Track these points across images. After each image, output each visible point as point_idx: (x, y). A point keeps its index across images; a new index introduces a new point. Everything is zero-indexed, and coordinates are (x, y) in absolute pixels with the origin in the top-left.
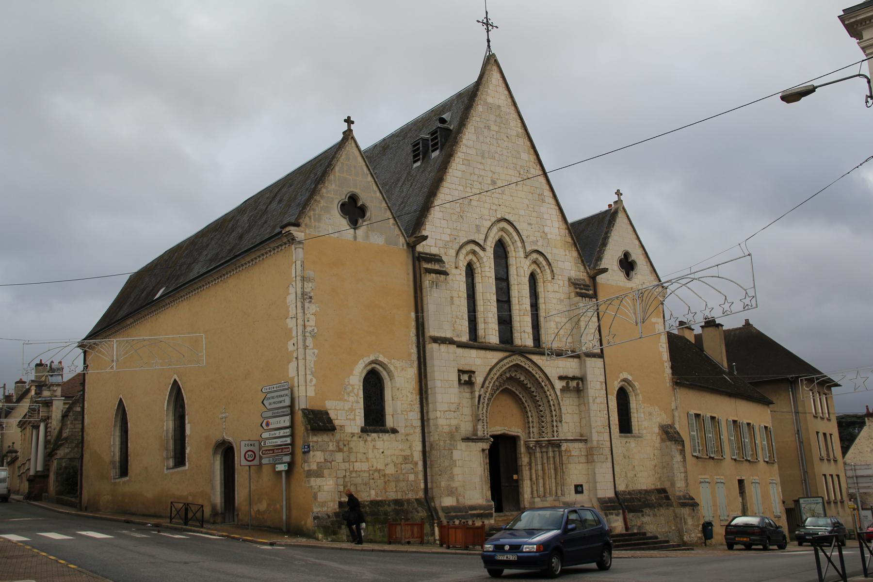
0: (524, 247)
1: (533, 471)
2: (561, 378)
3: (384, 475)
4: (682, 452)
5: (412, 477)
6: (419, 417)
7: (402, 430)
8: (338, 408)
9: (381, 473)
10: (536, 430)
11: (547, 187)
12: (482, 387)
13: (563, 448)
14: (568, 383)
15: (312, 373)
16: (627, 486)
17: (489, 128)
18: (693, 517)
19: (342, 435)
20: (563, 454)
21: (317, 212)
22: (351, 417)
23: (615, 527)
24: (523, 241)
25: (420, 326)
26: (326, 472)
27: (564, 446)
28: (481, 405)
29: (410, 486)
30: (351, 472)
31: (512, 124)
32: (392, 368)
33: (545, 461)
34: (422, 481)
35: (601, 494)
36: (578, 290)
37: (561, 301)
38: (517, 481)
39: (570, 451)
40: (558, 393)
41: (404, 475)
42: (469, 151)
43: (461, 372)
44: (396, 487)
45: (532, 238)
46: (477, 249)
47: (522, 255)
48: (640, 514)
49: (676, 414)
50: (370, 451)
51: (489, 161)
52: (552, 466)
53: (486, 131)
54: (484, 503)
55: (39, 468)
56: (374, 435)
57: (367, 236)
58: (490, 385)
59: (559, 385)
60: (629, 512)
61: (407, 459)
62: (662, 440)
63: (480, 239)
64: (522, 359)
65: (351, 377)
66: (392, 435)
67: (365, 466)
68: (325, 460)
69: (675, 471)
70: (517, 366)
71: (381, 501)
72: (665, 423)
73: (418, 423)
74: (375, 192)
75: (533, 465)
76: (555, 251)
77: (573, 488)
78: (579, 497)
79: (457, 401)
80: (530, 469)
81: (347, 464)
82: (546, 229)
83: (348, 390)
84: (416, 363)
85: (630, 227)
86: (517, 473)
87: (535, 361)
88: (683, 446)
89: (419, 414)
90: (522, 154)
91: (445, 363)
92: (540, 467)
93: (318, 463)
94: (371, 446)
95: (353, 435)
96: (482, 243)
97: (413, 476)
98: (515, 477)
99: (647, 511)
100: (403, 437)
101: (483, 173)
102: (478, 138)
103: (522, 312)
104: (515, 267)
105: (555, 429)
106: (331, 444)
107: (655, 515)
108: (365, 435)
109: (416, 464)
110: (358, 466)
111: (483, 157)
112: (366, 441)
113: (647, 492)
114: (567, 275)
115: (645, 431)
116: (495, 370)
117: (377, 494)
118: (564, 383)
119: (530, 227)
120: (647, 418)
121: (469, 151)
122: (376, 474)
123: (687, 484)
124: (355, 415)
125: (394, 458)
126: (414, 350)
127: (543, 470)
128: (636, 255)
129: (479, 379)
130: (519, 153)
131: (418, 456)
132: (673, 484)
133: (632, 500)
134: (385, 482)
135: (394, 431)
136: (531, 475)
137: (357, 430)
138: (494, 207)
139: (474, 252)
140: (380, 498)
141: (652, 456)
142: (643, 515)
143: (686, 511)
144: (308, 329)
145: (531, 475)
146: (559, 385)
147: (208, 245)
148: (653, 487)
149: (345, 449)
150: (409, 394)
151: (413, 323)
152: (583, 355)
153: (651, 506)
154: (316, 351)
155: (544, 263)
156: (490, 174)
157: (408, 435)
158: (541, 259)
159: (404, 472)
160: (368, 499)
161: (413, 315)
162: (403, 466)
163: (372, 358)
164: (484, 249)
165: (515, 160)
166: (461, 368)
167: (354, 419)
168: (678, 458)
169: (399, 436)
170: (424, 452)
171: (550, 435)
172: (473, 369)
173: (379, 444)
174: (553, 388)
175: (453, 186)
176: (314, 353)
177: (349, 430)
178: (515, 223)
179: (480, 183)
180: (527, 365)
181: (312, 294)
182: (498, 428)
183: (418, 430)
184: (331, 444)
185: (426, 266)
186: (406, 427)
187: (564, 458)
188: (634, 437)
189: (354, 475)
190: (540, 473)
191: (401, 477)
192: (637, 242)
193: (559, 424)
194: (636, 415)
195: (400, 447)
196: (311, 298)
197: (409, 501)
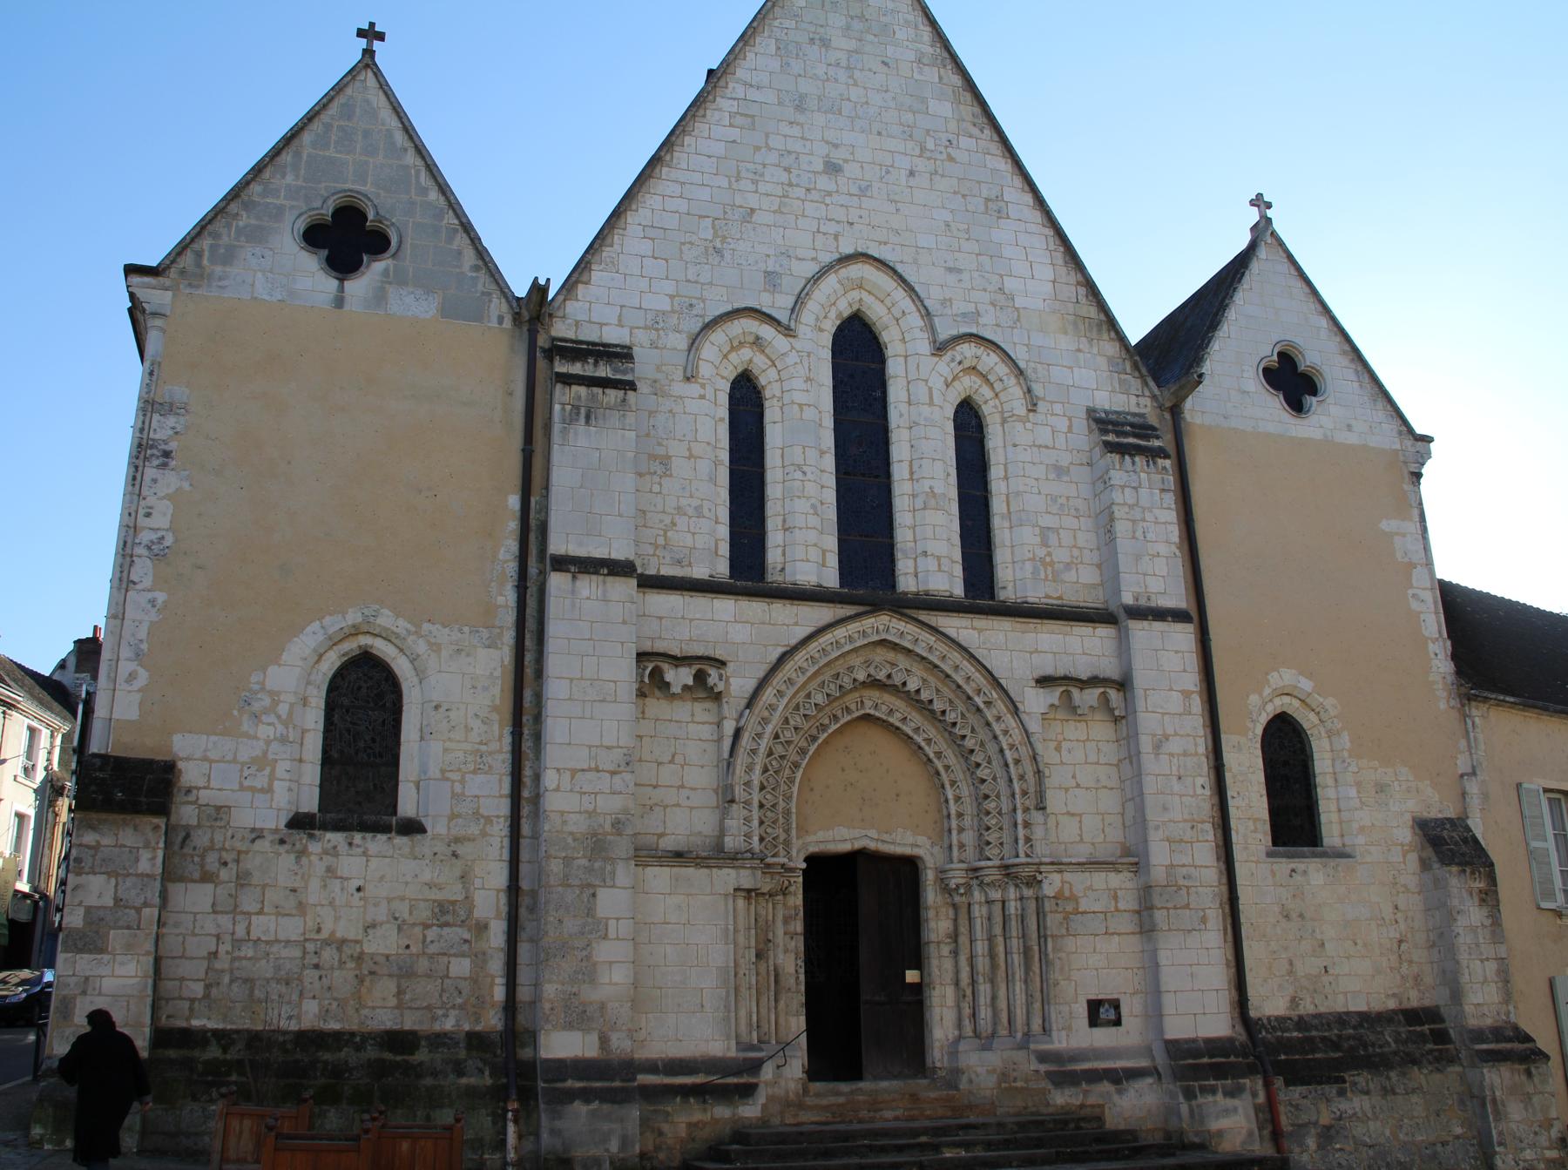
0: (932, 329)
1: (963, 959)
2: (1044, 681)
3: (359, 958)
4: (1489, 897)
5: (461, 967)
6: (506, 788)
7: (437, 827)
8: (212, 755)
9: (347, 951)
10: (969, 838)
11: (1018, 181)
12: (750, 704)
15: (138, 655)
16: (1294, 1001)
17: (825, 43)
18: (1527, 1099)
19: (218, 837)
20: (1048, 906)
21: (225, 240)
22: (260, 781)
23: (1220, 1133)
24: (927, 314)
25: (532, 529)
26: (116, 937)
27: (1052, 883)
29: (455, 995)
30: (237, 943)
31: (901, 35)
32: (422, 647)
33: (998, 930)
34: (500, 981)
35: (1178, 1028)
36: (1111, 438)
37: (1060, 471)
38: (918, 988)
39: (1074, 898)
40: (1034, 726)
41: (431, 957)
42: (753, 94)
43: (642, 656)
44: (400, 993)
45: (960, 307)
46: (767, 331)
47: (924, 347)
48: (1331, 1090)
49: (1473, 788)
50: (315, 884)
51: (820, 119)
52: (1015, 943)
53: (814, 51)
54: (733, 1053)
56: (335, 838)
57: (380, 297)
59: (1035, 702)
60: (1288, 1083)
61: (444, 912)
62: (1425, 865)
63: (779, 304)
64: (910, 628)
65: (272, 670)
66: (400, 841)
67: (292, 928)
68: (117, 900)
69: (1463, 957)
71: (337, 1036)
72: (1434, 814)
73: (504, 808)
74: (424, 191)
75: (964, 940)
76: (1037, 339)
77: (1082, 1010)
78: (1103, 1037)
79: (626, 740)
80: (955, 953)
81: (225, 921)
82: (1010, 284)
83: (256, 706)
84: (509, 637)
85: (1300, 284)
86: (918, 965)
87: (952, 632)
88: (1492, 879)
89: (507, 781)
90: (932, 103)
91: (592, 633)
92: (981, 947)
93: (88, 910)
94: (319, 867)
95: (257, 834)
96: (783, 316)
97: (466, 963)
98: (911, 976)
99: (1362, 1078)
100: (440, 847)
101: (797, 146)
102: (785, 66)
103: (919, 503)
104: (902, 382)
105: (1021, 832)
106: (145, 855)
107: (1387, 1091)
108: (300, 837)
109: (482, 928)
110: (263, 926)
111: (800, 108)
112: (302, 853)
113: (1365, 1018)
114: (1082, 401)
115: (1361, 840)
117: (325, 1013)
118: (1054, 695)
119: (951, 279)
120: (1367, 803)
121: (753, 94)
122: (329, 955)
123: (1507, 997)
124: (272, 777)
125: (403, 910)
126: (509, 597)
127: (992, 955)
128: (1315, 354)
129: (739, 684)
130: (924, 101)
131: (489, 901)
132: (1457, 995)
133: (1308, 1044)
134: (360, 980)
135: (412, 828)
136: (957, 972)
137: (272, 818)
138: (831, 228)
139: (757, 342)
140: (334, 1026)
141: (1387, 911)
142: (1342, 1093)
143: (1497, 1078)
144: (145, 537)
145: (957, 972)
148: (1392, 1004)
149: (224, 874)
150: (476, 724)
151: (513, 525)
152: (1122, 615)
153: (1376, 1063)
154: (161, 597)
155: (1002, 369)
156: (822, 150)
157: (457, 840)
158: (990, 360)
159: (432, 949)
160: (294, 1026)
161: (514, 501)
162: (431, 934)
163: (353, 617)
164: (788, 331)
165: (908, 117)
166: (647, 646)
167: (269, 790)
168: (1474, 915)
169: (424, 844)
170: (513, 888)
171: (1007, 850)
172: (719, 653)
173: (350, 865)
174: (1015, 710)
175: (697, 177)
176: (153, 602)
177: (244, 818)
178: (899, 268)
179: (787, 170)
180: (924, 642)
181: (173, 446)
182: (843, 832)
183: (500, 829)
184: (145, 855)
185: (562, 367)
186: (453, 816)
187: (1052, 921)
188: (1324, 855)
189: (247, 951)
190: (982, 963)
191: (423, 965)
192: (1324, 322)
193: (1037, 817)
194: (1331, 793)
195: (427, 876)
196: (167, 454)
197: (439, 1040)
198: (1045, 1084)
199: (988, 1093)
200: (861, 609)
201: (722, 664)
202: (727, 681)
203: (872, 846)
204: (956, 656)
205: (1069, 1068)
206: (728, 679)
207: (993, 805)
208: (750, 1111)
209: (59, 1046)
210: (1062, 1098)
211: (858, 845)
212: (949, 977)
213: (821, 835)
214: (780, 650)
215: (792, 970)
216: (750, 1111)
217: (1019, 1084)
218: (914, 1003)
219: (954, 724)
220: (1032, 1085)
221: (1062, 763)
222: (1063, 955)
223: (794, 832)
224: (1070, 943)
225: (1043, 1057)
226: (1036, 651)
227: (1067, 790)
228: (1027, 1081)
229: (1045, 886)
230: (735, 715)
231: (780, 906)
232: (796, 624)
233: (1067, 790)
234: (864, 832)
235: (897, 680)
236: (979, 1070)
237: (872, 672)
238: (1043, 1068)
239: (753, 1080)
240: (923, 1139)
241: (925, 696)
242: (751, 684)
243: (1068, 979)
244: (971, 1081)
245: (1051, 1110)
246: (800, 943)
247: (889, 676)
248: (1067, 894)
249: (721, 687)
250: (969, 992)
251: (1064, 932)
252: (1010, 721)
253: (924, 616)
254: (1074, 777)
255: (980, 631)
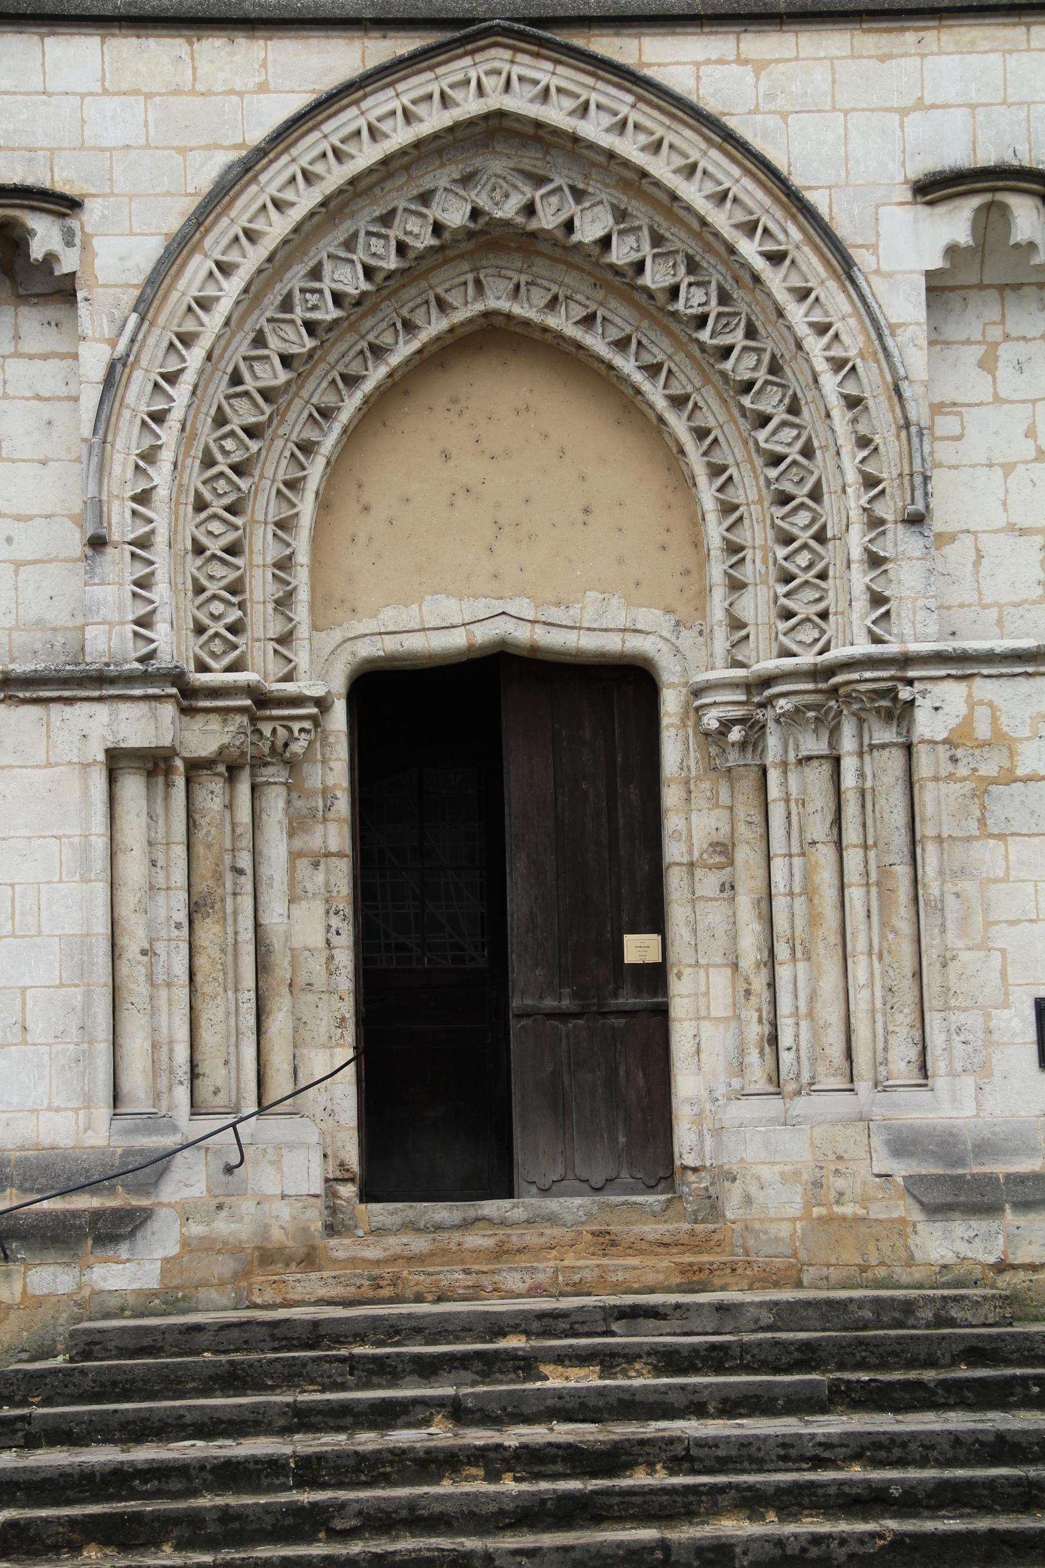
12: (145, 305)
13: (926, 724)
14: (991, 221)
20: (925, 763)
27: (941, 708)
28: (127, 440)
55: (335, 1254)
58: (216, 287)
64: (544, 72)
70: (495, 129)
75: (747, 856)
87: (678, 79)
98: (639, 948)
116: (273, 178)
118: (955, 223)
129: (113, 252)
146: (905, 246)
147: (331, 210)
180: (600, 119)
182: (451, 609)
193: (899, 542)
198: (905, 1209)
199: (784, 1230)
200: (404, 45)
201: (64, 205)
202: (86, 247)
203: (522, 635)
204: (690, 141)
205: (977, 1169)
206: (87, 238)
207: (803, 518)
208: (123, 1275)
209: (1007, 1206)
210: (945, 1245)
211: (484, 634)
212: (715, 950)
213: (389, 618)
214: (223, 159)
215: (317, 940)
216: (123, 1275)
217: (848, 1209)
218: (638, 1025)
219: (701, 321)
220: (877, 1211)
221: (997, 399)
222: (969, 887)
223: (301, 613)
224: (988, 856)
225: (903, 1144)
226: (920, 105)
227: (1008, 468)
228: (865, 1201)
229: (922, 716)
230: (107, 331)
231: (275, 803)
232: (263, 88)
233: (1008, 468)
234: (498, 606)
235: (548, 219)
236: (766, 1172)
237: (483, 202)
238: (901, 1169)
239: (144, 1202)
240: (514, 1342)
241: (621, 254)
242: (147, 251)
243: (984, 946)
244: (748, 1200)
245: (918, 1274)
246: (340, 877)
247: (530, 210)
248: (983, 731)
249: (68, 262)
250: (759, 983)
251: (973, 828)
252: (836, 301)
253: (578, 40)
254: (1030, 433)
255: (760, 66)
